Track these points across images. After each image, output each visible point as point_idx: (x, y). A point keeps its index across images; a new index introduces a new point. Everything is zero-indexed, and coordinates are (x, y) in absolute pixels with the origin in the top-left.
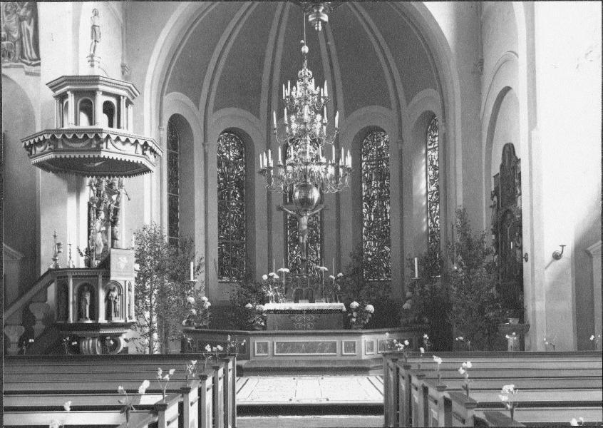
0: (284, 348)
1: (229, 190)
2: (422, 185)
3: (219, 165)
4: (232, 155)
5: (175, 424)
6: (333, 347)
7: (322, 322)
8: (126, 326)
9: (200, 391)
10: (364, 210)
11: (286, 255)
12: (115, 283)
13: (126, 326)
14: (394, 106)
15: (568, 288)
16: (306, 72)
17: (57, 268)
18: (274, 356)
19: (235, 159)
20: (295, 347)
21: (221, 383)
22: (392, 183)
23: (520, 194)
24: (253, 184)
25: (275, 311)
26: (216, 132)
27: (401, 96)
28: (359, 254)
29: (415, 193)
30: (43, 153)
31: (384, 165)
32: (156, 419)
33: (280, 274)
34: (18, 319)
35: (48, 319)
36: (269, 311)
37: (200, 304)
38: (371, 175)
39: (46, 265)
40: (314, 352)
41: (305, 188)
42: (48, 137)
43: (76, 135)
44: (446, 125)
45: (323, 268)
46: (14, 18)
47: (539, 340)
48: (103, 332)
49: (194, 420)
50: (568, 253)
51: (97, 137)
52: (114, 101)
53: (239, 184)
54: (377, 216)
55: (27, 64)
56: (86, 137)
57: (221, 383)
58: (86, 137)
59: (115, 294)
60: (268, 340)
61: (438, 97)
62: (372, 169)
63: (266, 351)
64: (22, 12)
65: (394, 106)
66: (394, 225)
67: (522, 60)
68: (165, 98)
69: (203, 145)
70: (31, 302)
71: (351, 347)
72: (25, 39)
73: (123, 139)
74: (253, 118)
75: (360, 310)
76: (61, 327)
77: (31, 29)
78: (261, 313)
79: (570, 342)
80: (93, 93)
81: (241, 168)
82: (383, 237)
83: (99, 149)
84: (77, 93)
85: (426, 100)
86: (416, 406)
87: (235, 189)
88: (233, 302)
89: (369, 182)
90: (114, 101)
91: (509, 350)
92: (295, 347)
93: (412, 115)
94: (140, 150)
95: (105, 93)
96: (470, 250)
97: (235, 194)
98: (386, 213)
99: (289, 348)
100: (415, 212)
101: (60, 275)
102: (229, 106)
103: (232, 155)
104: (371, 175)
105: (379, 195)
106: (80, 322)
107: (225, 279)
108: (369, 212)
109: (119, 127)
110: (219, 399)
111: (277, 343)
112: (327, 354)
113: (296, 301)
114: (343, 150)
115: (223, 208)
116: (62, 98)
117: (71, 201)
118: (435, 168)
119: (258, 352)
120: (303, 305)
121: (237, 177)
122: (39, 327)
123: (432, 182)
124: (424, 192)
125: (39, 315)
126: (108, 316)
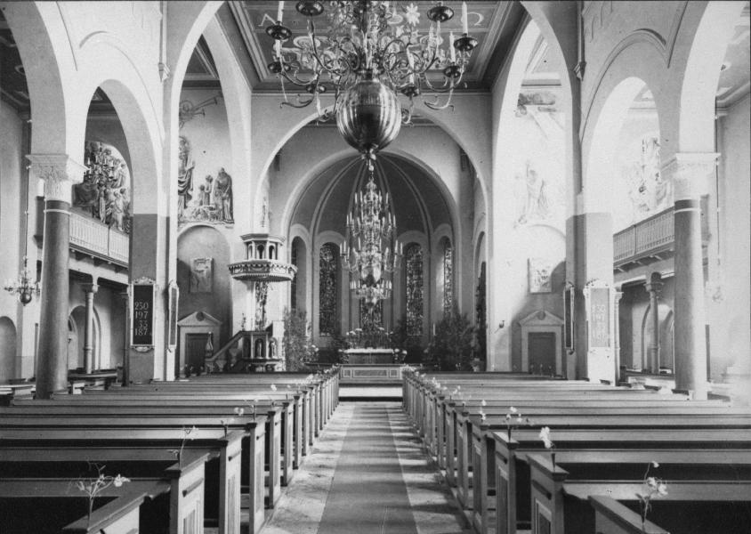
0: (358, 373)
2: (441, 279)
3: (321, 265)
4: (328, 259)
6: (385, 373)
7: (382, 360)
8: (278, 360)
9: (295, 406)
10: (408, 293)
11: (360, 319)
12: (274, 339)
13: (278, 360)
15: (507, 341)
16: (372, 185)
17: (244, 331)
20: (365, 373)
21: (300, 409)
22: (425, 276)
25: (353, 354)
26: (318, 246)
27: (431, 227)
28: (404, 317)
29: (438, 285)
30: (239, 273)
32: (249, 434)
33: (357, 332)
34: (223, 356)
35: (239, 356)
36: (350, 354)
37: (312, 349)
39: (236, 329)
41: (370, 298)
43: (255, 265)
44: (454, 246)
45: (381, 328)
46: (220, 198)
47: (492, 367)
48: (268, 363)
49: (234, 477)
51: (268, 266)
52: (274, 245)
53: (332, 276)
54: (415, 297)
56: (262, 266)
57: (300, 409)
58: (262, 266)
59: (273, 344)
60: (351, 369)
61: (450, 228)
64: (224, 195)
66: (425, 302)
67: (487, 217)
70: (230, 348)
71: (394, 373)
72: (226, 209)
75: (399, 353)
76: (245, 361)
77: (229, 204)
78: (346, 354)
79: (507, 368)
80: (265, 242)
81: (334, 267)
82: (419, 310)
83: (268, 272)
84: (256, 242)
85: (443, 230)
86: (449, 427)
88: (329, 348)
90: (274, 245)
91: (84, 305)
92: (365, 373)
93: (437, 237)
95: (271, 242)
96: (460, 321)
100: (437, 296)
101: (244, 333)
103: (328, 259)
105: (417, 283)
107: (323, 334)
109: (276, 258)
113: (366, 347)
114: (397, 242)
115: (322, 291)
116: (248, 244)
117: (249, 294)
118: (449, 270)
120: (370, 350)
122: (234, 360)
123: (448, 277)
124: (443, 283)
125: (234, 355)
126: (270, 355)
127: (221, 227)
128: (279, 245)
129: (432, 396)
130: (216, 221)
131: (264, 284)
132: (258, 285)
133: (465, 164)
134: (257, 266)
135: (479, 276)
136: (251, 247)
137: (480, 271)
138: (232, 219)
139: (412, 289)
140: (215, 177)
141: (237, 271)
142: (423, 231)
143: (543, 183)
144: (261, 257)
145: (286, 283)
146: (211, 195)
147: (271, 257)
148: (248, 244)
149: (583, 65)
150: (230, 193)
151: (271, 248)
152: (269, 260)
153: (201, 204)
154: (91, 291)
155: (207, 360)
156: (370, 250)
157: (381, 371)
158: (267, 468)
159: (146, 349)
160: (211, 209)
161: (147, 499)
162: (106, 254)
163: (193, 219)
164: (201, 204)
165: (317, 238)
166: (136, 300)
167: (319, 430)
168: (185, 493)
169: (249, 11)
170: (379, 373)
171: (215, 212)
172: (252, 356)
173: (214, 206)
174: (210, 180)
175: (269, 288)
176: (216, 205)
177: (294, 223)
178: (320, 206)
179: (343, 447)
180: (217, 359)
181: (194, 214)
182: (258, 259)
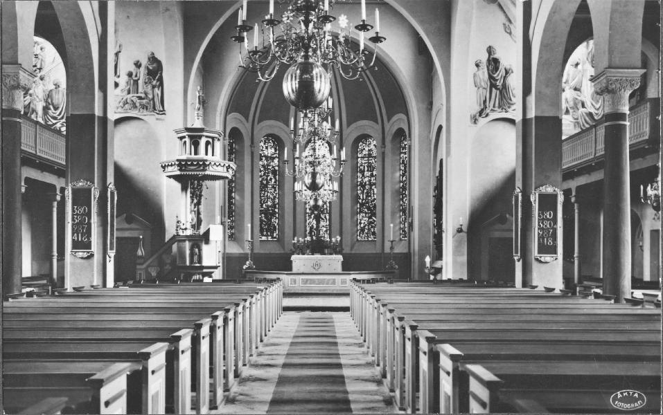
1: (267, 176)
5: (121, 406)
6: (334, 282)
10: (359, 192)
42: (177, 163)
44: (410, 140)
46: (150, 86)
50: (465, 228)
52: (211, 140)
55: (158, 114)
57: (219, 333)
63: (295, 283)
64: (154, 83)
68: (228, 117)
69: (251, 146)
72: (156, 99)
73: (217, 164)
77: (159, 93)
85: (398, 121)
89: (362, 172)
90: (211, 140)
94: (225, 170)
95: (207, 137)
97: (271, 179)
98: (374, 194)
99: (308, 282)
108: (363, 193)
110: (218, 349)
121: (273, 167)
122: (168, 267)
127: (150, 118)
128: (216, 141)
129: (389, 315)
130: (145, 112)
131: (198, 182)
132: (192, 184)
133: (421, 49)
134: (192, 164)
135: (437, 174)
136: (185, 142)
137: (438, 169)
138: (164, 110)
139: (364, 189)
140: (144, 62)
141: (170, 169)
142: (376, 122)
143: (507, 72)
144: (196, 153)
145: (221, 182)
146: (140, 82)
148: (181, 138)
150: (161, 80)
151: (207, 143)
152: (205, 157)
153: (129, 93)
154: (55, 200)
155: (138, 267)
157: (329, 280)
158: (211, 376)
159: (85, 255)
160: (140, 98)
161: (127, 375)
162: (34, 152)
163: (120, 110)
164: (129, 93)
166: (74, 204)
167: (267, 332)
168: (153, 372)
169: (288, 124)
171: (144, 101)
172: (188, 263)
173: (143, 95)
174: (138, 65)
175: (204, 188)
176: (146, 94)
177: (230, 113)
179: (275, 393)
180: (148, 266)
181: (121, 104)
182: (193, 156)
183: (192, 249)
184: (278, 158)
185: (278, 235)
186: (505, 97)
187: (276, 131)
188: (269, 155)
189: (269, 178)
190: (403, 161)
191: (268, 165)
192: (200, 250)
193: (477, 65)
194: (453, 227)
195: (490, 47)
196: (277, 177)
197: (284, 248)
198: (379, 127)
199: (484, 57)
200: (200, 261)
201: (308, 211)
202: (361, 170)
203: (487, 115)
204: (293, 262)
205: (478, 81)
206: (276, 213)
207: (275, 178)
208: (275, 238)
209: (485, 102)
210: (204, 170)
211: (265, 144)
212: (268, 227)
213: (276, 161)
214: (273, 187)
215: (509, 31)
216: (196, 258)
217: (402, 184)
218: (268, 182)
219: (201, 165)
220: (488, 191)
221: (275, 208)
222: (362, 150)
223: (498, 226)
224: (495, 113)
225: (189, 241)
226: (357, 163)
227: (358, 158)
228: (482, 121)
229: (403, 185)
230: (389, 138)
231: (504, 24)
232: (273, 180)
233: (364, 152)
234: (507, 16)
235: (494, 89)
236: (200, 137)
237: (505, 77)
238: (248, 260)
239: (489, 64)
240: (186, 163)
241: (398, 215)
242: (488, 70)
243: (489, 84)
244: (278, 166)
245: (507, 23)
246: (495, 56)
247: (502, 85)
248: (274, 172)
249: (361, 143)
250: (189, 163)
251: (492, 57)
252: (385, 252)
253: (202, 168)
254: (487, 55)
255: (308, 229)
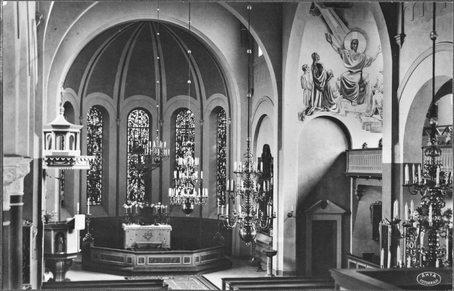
1: (93, 144)
14: (198, 97)
18: (147, 265)
19: (97, 124)
20: (159, 260)
23: (273, 177)
24: (108, 141)
31: (191, 132)
38: (182, 137)
40: (169, 263)
51: (72, 160)
56: (66, 159)
62: (183, 134)
65: (198, 97)
69: (80, 118)
71: (187, 260)
74: (109, 98)
85: (217, 100)
87: (96, 144)
97: (95, 147)
99: (155, 261)
102: (97, 91)
104: (182, 137)
106: (57, 253)
111: (149, 258)
112: (175, 264)
119: (139, 263)
121: (97, 136)
134: (60, 160)
147: (71, 148)
149: (403, 36)
156: (54, 41)
165: (85, 100)
170: (173, 260)
172: (53, 252)
178: (89, 68)
183: (56, 238)
184: (102, 127)
185: (101, 199)
186: (327, 98)
187: (101, 103)
188: (94, 124)
189: (94, 146)
190: (220, 135)
191: (93, 134)
192: (65, 239)
193: (304, 69)
194: (285, 211)
195: (314, 54)
196: (101, 145)
197: (108, 213)
198: (198, 102)
199: (310, 62)
200: (64, 249)
201: (129, 176)
202: (178, 140)
203: (312, 113)
204: (127, 233)
205: (305, 83)
206: (99, 178)
207: (99, 146)
208: (99, 202)
209: (310, 101)
210: (71, 165)
211: (90, 114)
212: (93, 192)
213: (100, 130)
214: (97, 154)
215: (330, 41)
216: (60, 247)
217: (219, 156)
218: (93, 150)
219: (68, 161)
220: (312, 179)
221: (99, 174)
222: (180, 122)
223: (320, 210)
224: (319, 112)
225: (54, 230)
226: (176, 133)
227: (176, 128)
228: (308, 118)
229: (220, 157)
230: (207, 115)
231: (326, 34)
232: (97, 148)
233: (182, 124)
234: (328, 27)
235: (317, 91)
236: (65, 133)
237: (326, 81)
238: (87, 233)
239: (314, 68)
240: (55, 159)
241: (215, 184)
242: (313, 74)
243: (313, 86)
244: (102, 134)
245: (329, 34)
246: (320, 62)
247: (325, 87)
248: (98, 141)
249: (179, 115)
250: (58, 159)
251: (316, 62)
252: (203, 217)
253: (69, 164)
254: (312, 61)
255: (129, 193)
